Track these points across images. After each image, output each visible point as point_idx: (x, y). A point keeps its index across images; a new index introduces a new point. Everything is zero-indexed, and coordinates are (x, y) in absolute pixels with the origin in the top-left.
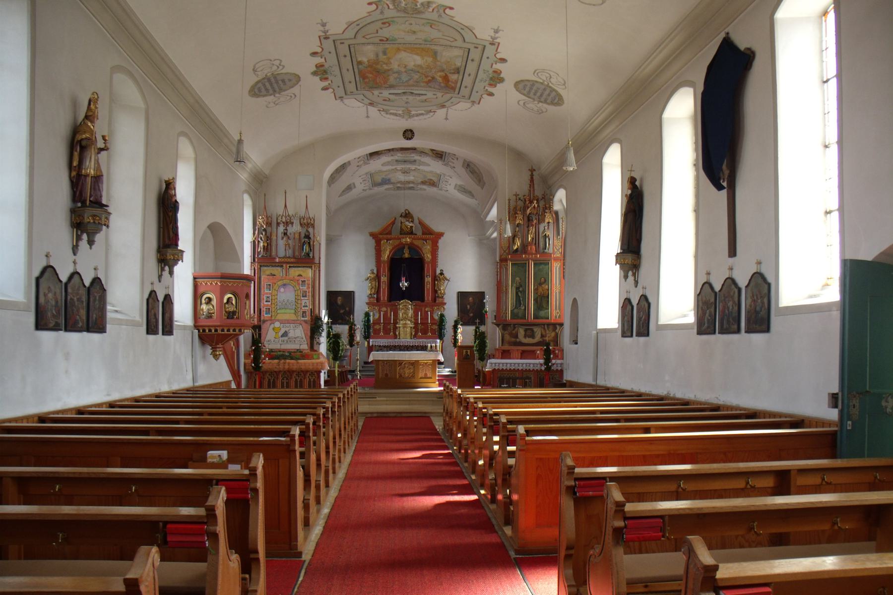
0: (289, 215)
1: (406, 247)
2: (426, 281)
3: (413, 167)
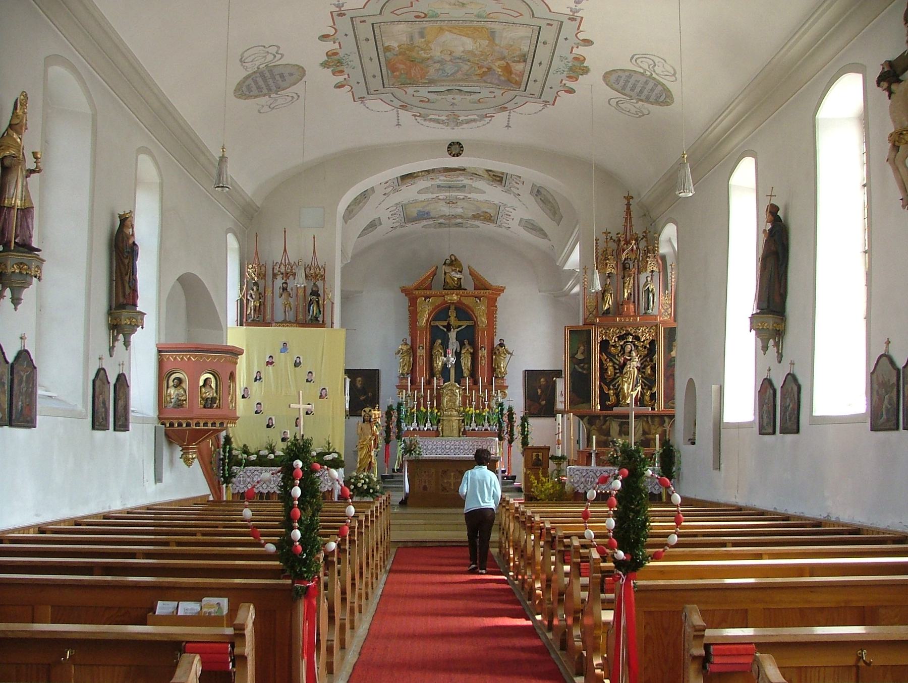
0: (289, 264)
1: (452, 307)
2: (480, 355)
3: (461, 195)
